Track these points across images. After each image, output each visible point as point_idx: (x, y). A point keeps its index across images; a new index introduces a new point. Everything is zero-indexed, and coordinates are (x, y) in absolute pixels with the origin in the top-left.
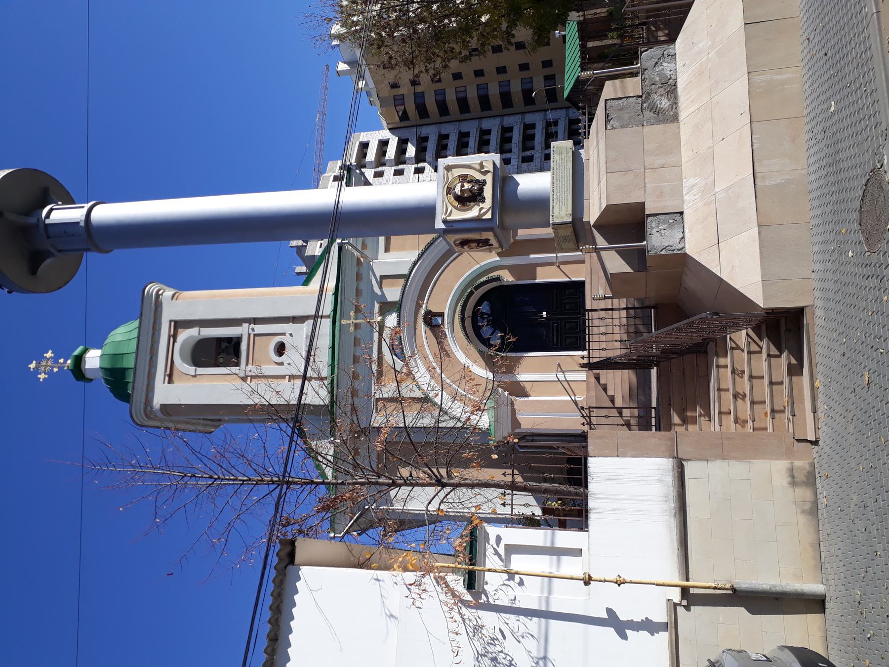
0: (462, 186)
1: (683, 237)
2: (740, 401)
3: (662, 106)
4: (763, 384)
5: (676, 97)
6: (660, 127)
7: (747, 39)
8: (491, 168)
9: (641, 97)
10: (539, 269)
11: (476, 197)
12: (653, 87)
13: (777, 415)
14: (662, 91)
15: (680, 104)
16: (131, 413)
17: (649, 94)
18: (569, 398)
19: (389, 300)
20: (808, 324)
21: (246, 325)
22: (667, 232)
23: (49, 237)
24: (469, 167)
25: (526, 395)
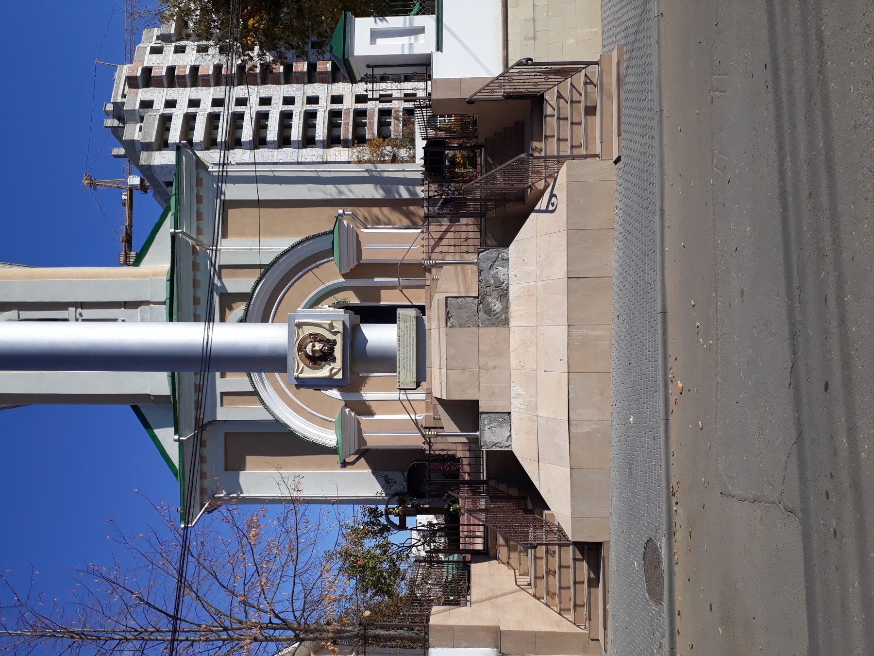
0: (313, 346)
2: (551, 577)
4: (569, 573)
5: (507, 302)
6: (493, 330)
7: (569, 292)
9: (477, 297)
10: (383, 292)
11: (326, 357)
12: (488, 289)
13: (578, 609)
14: (495, 294)
15: (511, 310)
17: (484, 296)
18: (407, 417)
19: (229, 291)
20: (604, 557)
22: (497, 430)
25: (371, 413)
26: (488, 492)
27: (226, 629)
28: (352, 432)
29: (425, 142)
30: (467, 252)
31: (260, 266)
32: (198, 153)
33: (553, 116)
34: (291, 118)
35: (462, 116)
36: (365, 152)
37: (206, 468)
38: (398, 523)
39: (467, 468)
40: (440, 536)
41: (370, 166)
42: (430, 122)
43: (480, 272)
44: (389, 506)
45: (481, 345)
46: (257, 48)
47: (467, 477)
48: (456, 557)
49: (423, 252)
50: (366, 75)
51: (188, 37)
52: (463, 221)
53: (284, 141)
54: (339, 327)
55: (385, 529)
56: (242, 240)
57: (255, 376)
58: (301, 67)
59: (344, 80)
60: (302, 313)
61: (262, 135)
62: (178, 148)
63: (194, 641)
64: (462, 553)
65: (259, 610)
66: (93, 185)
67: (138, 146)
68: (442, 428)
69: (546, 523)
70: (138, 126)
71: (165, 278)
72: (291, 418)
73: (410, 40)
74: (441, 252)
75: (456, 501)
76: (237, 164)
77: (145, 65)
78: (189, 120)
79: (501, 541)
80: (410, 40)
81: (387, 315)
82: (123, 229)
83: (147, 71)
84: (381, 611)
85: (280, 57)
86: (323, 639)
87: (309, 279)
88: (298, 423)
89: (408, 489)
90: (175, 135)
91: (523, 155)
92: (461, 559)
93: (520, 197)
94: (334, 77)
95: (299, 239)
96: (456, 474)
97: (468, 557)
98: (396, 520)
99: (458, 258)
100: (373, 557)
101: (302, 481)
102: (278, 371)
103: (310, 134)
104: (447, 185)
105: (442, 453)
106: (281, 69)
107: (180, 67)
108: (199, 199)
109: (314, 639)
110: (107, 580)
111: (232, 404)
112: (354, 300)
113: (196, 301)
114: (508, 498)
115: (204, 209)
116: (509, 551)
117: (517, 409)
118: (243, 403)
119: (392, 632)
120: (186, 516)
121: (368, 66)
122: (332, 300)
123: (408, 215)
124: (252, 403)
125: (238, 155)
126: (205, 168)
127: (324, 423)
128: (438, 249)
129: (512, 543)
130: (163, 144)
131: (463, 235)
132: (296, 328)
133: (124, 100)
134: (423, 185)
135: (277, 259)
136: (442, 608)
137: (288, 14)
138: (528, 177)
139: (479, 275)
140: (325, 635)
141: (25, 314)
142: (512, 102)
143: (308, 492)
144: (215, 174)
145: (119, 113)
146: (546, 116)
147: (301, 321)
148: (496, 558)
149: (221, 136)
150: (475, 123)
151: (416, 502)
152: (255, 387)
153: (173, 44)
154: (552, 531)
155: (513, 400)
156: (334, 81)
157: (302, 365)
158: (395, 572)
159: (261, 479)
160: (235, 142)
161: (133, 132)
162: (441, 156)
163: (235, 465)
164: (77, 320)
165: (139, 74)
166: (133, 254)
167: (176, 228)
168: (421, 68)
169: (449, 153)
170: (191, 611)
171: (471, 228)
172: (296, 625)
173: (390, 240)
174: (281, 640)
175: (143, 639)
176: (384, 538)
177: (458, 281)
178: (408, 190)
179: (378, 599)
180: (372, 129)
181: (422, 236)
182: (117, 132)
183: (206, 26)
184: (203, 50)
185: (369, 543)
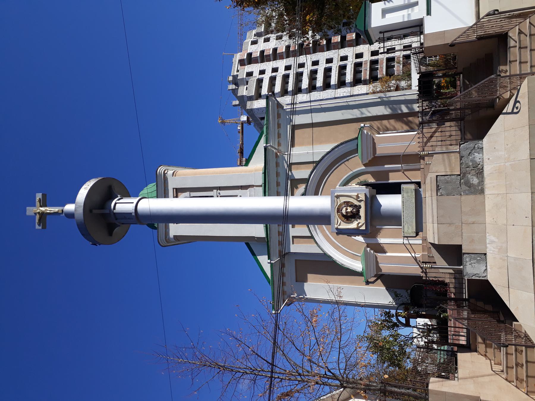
0: (347, 209)
1: (486, 269)
3: (474, 182)
5: (483, 177)
6: (471, 197)
8: (364, 198)
9: (459, 175)
10: (391, 174)
11: (355, 215)
12: (468, 169)
15: (485, 183)
16: (158, 241)
17: (465, 174)
18: (409, 255)
21: (215, 191)
22: (476, 265)
23: (116, 219)
24: (350, 196)
25: (385, 252)
26: (469, 307)
27: (300, 375)
28: (372, 263)
29: (419, 75)
30: (451, 145)
31: (313, 162)
32: (279, 99)
33: (516, 46)
34: (346, 69)
35: (445, 55)
36: (378, 86)
37: (285, 280)
38: (404, 322)
39: (453, 290)
40: (434, 333)
41: (382, 95)
42: (421, 62)
43: (461, 158)
44: (398, 311)
45: (463, 208)
46: (310, 33)
47: (453, 296)
48: (446, 347)
49: (419, 147)
50: (379, 38)
51: (272, 32)
52: (448, 124)
53: (327, 86)
54: (362, 197)
55: (395, 325)
56: (303, 147)
57: (311, 227)
58: (337, 39)
59: (364, 43)
60: (339, 190)
61: (313, 84)
62: (267, 97)
63: (282, 379)
64: (451, 346)
65: (319, 366)
66: (223, 123)
67: (245, 99)
68: (435, 263)
69: (515, 331)
70: (245, 87)
71: (261, 172)
72: (333, 253)
73: (408, 11)
74: (432, 146)
75: (445, 311)
76: (300, 103)
77: (248, 52)
78: (273, 80)
79: (480, 340)
80: (408, 11)
81: (394, 189)
82: (239, 145)
83: (250, 55)
84: (394, 377)
85: (324, 35)
86: (358, 389)
87: (342, 168)
88: (337, 256)
89: (411, 301)
90: (265, 91)
91: (493, 76)
92: (450, 349)
93: (491, 105)
94: (357, 42)
95: (336, 144)
96: (445, 294)
97: (456, 349)
98: (403, 320)
99: (444, 149)
100: (388, 342)
101: (342, 291)
102: (325, 224)
103: (342, 79)
104: (434, 101)
105: (434, 279)
106: (325, 42)
107: (267, 50)
108: (279, 126)
109: (352, 388)
110: (236, 339)
111: (298, 243)
112: (372, 180)
113: (278, 184)
114: (485, 312)
115: (281, 131)
116: (486, 347)
117: (491, 251)
118: (305, 243)
119: (403, 391)
120: (276, 307)
121: (381, 33)
122: (357, 180)
123: (408, 123)
124: (310, 243)
125: (301, 97)
126: (282, 107)
127: (354, 257)
128: (429, 144)
129: (488, 342)
130: (259, 96)
131: (448, 134)
132: (336, 199)
133: (238, 73)
134: (418, 103)
135: (323, 158)
136: (437, 379)
137: (329, 8)
138: (496, 91)
139: (461, 160)
140: (359, 386)
141: (193, 194)
142: (483, 41)
143: (346, 298)
144: (287, 110)
145: (236, 82)
146: (510, 47)
147: (339, 194)
148: (476, 351)
149: (290, 88)
150: (454, 58)
151: (417, 310)
152: (311, 234)
153: (263, 37)
154: (520, 337)
155: (488, 245)
156: (357, 44)
157: (340, 221)
158: (403, 353)
159: (317, 288)
160: (298, 90)
161: (243, 91)
162: (431, 83)
163: (302, 279)
164: (218, 196)
165: (245, 57)
166: (244, 159)
167: (267, 143)
168: (417, 27)
169: (436, 81)
170: (280, 361)
171: (453, 128)
172: (341, 378)
173: (396, 140)
174: (332, 386)
175: (255, 374)
176: (395, 331)
177: (445, 165)
178: (407, 107)
179: (391, 368)
180: (382, 71)
181: (418, 136)
182: (235, 91)
183: (281, 24)
184: (279, 38)
185: (386, 333)
